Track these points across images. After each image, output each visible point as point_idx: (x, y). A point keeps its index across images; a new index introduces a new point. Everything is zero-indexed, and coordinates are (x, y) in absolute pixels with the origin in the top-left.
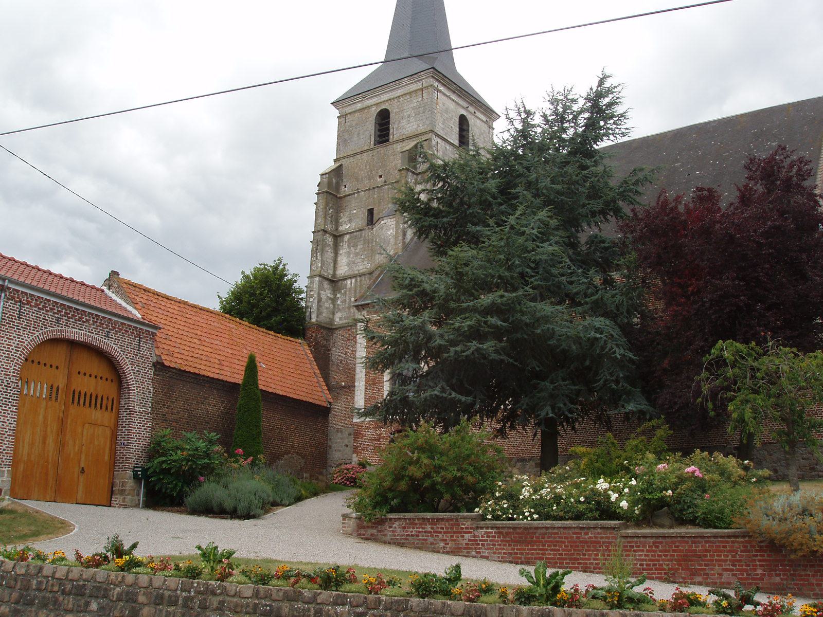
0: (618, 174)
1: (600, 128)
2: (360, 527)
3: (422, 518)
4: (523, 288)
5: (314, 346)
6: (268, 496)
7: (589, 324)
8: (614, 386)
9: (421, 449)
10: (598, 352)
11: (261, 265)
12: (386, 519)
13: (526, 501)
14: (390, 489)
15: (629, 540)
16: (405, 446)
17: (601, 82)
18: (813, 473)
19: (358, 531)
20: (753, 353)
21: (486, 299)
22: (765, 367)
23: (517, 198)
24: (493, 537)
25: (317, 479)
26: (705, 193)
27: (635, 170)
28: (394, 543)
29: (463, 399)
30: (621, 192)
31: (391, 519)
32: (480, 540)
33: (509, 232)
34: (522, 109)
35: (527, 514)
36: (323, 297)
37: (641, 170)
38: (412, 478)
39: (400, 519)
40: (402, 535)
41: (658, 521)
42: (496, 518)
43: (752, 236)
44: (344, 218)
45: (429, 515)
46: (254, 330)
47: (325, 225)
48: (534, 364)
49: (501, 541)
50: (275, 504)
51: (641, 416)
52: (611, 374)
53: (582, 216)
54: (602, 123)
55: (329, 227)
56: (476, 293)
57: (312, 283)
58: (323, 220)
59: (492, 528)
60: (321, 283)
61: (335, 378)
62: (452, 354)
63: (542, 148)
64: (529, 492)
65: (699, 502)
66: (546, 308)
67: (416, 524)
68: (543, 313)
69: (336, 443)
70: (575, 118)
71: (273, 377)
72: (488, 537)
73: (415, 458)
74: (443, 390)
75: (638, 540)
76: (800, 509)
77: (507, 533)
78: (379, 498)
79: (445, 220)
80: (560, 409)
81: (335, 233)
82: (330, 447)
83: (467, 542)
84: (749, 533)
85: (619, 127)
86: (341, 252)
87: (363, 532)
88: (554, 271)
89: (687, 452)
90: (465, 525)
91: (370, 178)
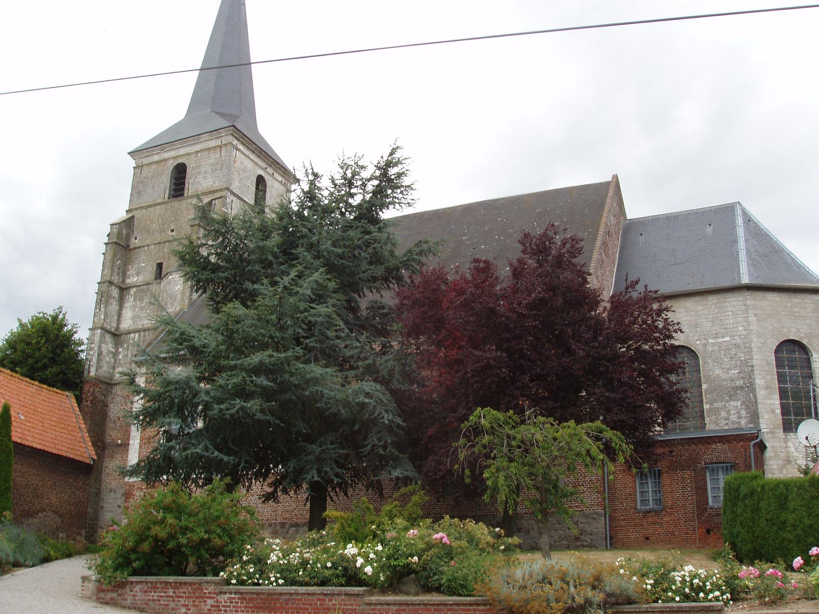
0: (403, 245)
1: (387, 196)
2: (100, 590)
3: (165, 582)
4: (294, 349)
5: (91, 401)
6: (8, 555)
7: (359, 388)
8: (382, 452)
9: (167, 509)
10: (366, 416)
11: (40, 313)
12: (127, 582)
13: (274, 566)
14: (134, 550)
15: (373, 607)
16: (150, 505)
17: (391, 154)
18: (578, 543)
19: (97, 595)
20: (511, 421)
21: (256, 358)
22: (520, 436)
23: (297, 258)
24: (236, 603)
25: (75, 540)
26: (482, 265)
27: (420, 241)
28: (134, 608)
29: (226, 458)
30: (405, 261)
31: (132, 583)
32: (223, 606)
33: (282, 292)
34: (310, 171)
35: (273, 579)
36: (104, 351)
37: (426, 242)
38: (156, 539)
39: (141, 582)
40: (144, 599)
41: (405, 588)
42: (242, 583)
43: (516, 308)
44: (131, 271)
45: (172, 579)
46: (16, 380)
47: (111, 277)
48: (302, 427)
49: (245, 607)
50: (17, 565)
51: (407, 481)
52: (380, 440)
53: (362, 280)
54: (389, 192)
55: (116, 279)
56: (246, 351)
57: (93, 335)
58: (110, 271)
59: (235, 593)
60: (102, 336)
61: (111, 436)
62: (216, 412)
63: (327, 211)
64: (277, 556)
65: (445, 569)
66: (316, 370)
67: (158, 588)
68: (312, 375)
69: (108, 503)
70: (364, 185)
71: (32, 430)
72: (231, 602)
73: (159, 518)
74: (206, 449)
75: (407, 608)
76: (540, 577)
77: (250, 599)
78: (121, 560)
79: (222, 275)
80: (326, 473)
81: (122, 285)
82: (102, 507)
83: (209, 607)
84: (488, 600)
85: (405, 197)
86: (126, 305)
87: (102, 595)
88: (331, 334)
89: (437, 519)
90: (208, 589)
91: (162, 231)
